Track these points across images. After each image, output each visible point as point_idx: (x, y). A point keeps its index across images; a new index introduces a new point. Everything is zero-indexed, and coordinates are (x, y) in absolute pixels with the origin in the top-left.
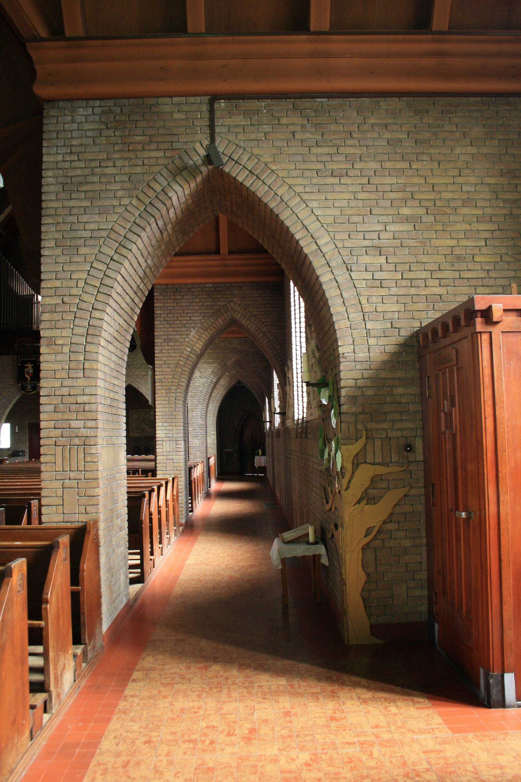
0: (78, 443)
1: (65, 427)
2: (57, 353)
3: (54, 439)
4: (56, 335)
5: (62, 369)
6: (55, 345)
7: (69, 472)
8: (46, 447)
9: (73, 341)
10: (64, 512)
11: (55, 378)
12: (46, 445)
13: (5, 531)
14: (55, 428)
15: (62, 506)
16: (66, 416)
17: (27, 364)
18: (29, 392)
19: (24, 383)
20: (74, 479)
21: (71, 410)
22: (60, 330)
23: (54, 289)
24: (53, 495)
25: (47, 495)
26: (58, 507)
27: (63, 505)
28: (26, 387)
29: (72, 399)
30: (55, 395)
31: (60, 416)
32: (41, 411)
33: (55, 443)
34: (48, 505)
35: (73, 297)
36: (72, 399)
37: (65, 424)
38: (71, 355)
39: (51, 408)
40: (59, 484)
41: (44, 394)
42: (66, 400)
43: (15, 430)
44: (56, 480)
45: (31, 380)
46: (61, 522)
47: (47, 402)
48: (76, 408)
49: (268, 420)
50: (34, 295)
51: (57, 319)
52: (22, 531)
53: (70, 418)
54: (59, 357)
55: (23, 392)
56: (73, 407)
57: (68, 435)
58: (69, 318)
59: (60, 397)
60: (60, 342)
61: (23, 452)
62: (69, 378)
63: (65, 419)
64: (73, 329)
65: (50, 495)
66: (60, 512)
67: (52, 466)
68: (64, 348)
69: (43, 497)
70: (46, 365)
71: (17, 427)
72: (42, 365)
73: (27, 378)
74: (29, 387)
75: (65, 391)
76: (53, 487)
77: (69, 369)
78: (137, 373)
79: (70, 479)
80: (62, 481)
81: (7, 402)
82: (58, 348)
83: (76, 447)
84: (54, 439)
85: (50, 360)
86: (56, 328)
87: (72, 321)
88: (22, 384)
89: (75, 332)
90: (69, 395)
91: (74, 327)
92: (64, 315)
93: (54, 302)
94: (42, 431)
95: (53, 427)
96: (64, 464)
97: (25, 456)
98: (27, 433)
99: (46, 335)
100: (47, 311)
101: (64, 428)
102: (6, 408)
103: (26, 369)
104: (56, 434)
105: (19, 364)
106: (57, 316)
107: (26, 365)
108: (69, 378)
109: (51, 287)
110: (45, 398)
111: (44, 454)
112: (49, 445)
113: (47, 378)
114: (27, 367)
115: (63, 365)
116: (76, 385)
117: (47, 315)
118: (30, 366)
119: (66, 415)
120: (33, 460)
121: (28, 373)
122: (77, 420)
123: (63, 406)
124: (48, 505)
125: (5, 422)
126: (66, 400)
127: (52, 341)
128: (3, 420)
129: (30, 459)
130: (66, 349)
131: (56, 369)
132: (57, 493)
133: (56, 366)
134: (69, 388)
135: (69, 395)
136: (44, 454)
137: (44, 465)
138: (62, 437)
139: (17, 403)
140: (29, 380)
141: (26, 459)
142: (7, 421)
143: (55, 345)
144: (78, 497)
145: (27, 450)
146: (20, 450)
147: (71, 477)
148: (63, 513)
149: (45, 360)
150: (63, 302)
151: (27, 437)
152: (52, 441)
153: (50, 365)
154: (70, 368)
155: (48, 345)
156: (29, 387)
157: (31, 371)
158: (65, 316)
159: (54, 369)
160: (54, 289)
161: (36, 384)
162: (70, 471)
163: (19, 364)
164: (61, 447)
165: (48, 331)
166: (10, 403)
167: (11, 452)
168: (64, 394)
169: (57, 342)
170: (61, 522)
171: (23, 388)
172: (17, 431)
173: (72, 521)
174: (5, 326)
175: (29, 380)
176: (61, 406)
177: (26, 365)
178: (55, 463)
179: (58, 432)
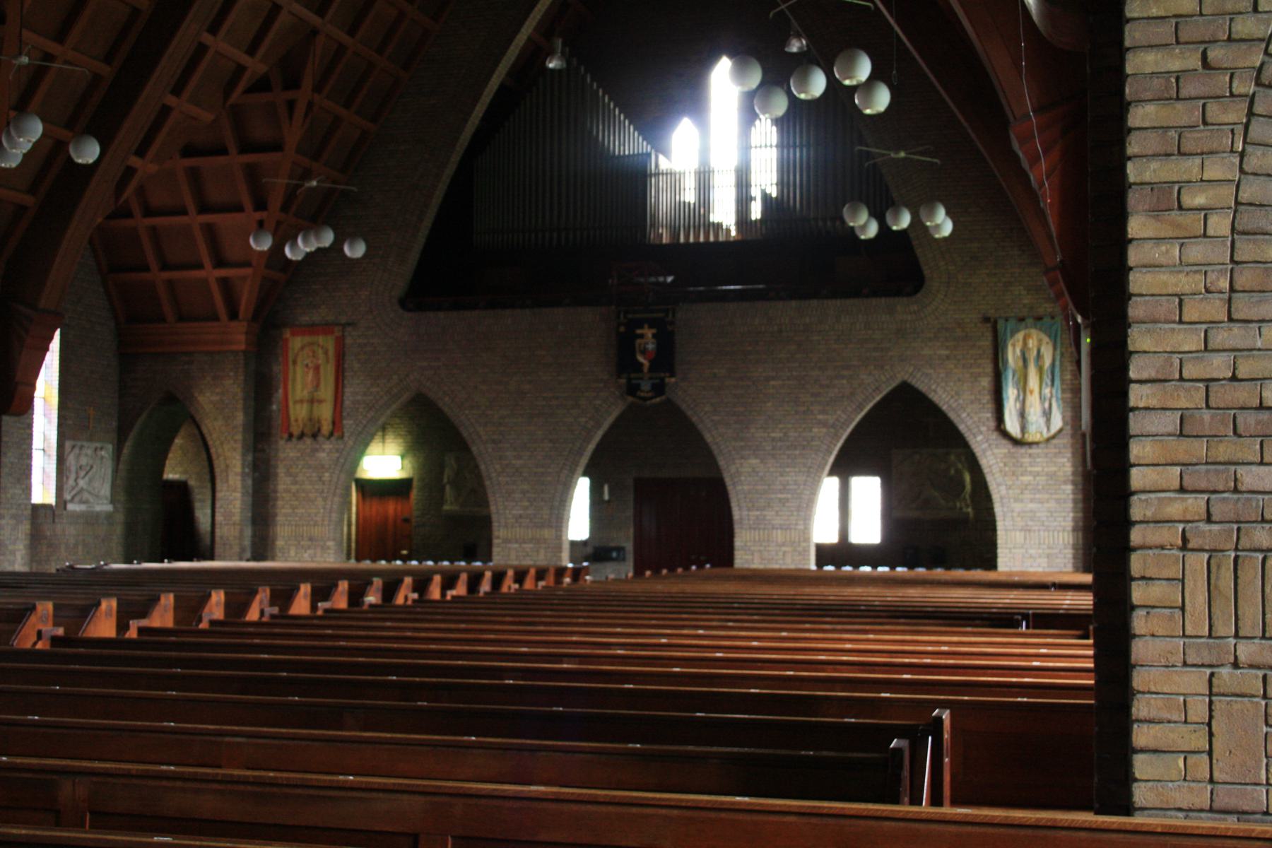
0: (1265, 545)
1: (1221, 488)
2: (1183, 240)
3: (1180, 527)
4: (1185, 178)
5: (1208, 291)
6: (1180, 208)
7: (1232, 641)
8: (1150, 552)
9: (1245, 196)
10: (1216, 775)
11: (1181, 322)
12: (1150, 548)
13: (1022, 832)
14: (1182, 490)
15: (1205, 757)
16: (1224, 451)
17: (642, 327)
18: (645, 399)
19: (633, 376)
20: (1251, 666)
21: (1241, 430)
22: (1198, 160)
23: (1173, 21)
24: (1175, 718)
25: (1153, 714)
26: (1192, 759)
27: (1210, 753)
28: (638, 387)
29: (1244, 395)
30: (1181, 379)
31: (1199, 449)
32: (1132, 432)
33: (1185, 539)
34: (1155, 751)
35: (1244, 46)
36: (1244, 395)
37: (1221, 480)
38: (1238, 245)
39: (1170, 422)
40: (1195, 681)
41: (1145, 376)
42: (1223, 394)
43: (602, 493)
44: (1185, 664)
45: (651, 369)
46: (1202, 810)
47: (1153, 402)
48: (1258, 422)
49: (448, 488)
50: (649, 155)
51: (1185, 121)
52: (1083, 834)
53: (1239, 456)
54: (1196, 252)
55: (630, 399)
56: (1248, 421)
57: (1232, 516)
58: (1231, 117)
59: (1201, 385)
60: (1199, 199)
61: (620, 549)
62: (1231, 319)
63: (1221, 459)
64: (1242, 155)
65: (1167, 716)
66: (1199, 776)
67: (1171, 618)
68: (1213, 220)
69: (1138, 721)
70: (1149, 277)
71: (583, 487)
72: (1132, 276)
73: (641, 365)
74: (646, 386)
75: (1218, 366)
76: (1174, 689)
77: (1232, 290)
78: (927, 352)
79: (1236, 665)
80: (1208, 671)
81: (592, 423)
82: (1193, 222)
83: (1260, 556)
84: (1180, 527)
85: (1163, 260)
86: (1180, 153)
87: (1239, 130)
88: (629, 380)
89: (1252, 163)
90: (1234, 378)
91: (1249, 149)
92: (1209, 107)
93: (1176, 65)
94: (1134, 499)
95: (1176, 485)
96: (1217, 612)
97: (624, 559)
98: (631, 504)
99: (1147, 177)
100: (1148, 95)
101: (1215, 492)
102: (587, 440)
103: (638, 341)
104: (1186, 510)
105: (622, 329)
106: (1183, 114)
107: (639, 331)
108: (1231, 319)
109: (1162, 14)
110: (1146, 389)
111: (1143, 578)
112: (1163, 548)
113: (1155, 321)
114: (642, 336)
115: (1212, 276)
116: (1259, 344)
117: (1150, 108)
118: (649, 333)
119: (1221, 448)
120: (648, 573)
121: (644, 352)
122: (1262, 463)
123: (1212, 417)
124: (1155, 751)
125: (831, 473)
126: (1223, 394)
127: (1169, 199)
128: (581, 469)
129: (639, 572)
130: (1220, 225)
131: (1187, 289)
132: (1190, 712)
133: (1185, 283)
134: (1232, 355)
135: (1234, 378)
136: (1143, 578)
137: (1142, 612)
138: (1209, 520)
139: (614, 426)
140: (646, 369)
141: (627, 569)
142: (584, 474)
143: (1180, 208)
144: (1265, 729)
145: (629, 546)
146: (612, 544)
147: (1242, 658)
148: (1211, 781)
149: (1145, 262)
150: (1205, 63)
151: (630, 513)
152: (1172, 535)
153: (1164, 277)
154: (1237, 287)
155: (1156, 211)
156: (646, 386)
157: (651, 347)
158: (1214, 110)
159: (1178, 290)
160: (1173, 21)
161: (662, 380)
162: (1236, 636)
163: (622, 329)
164: (1206, 556)
165: (1154, 165)
166: (598, 425)
167: (589, 550)
168: (1215, 375)
169: (1188, 201)
170: (1202, 810)
171: (632, 390)
172: (606, 497)
173: (1246, 808)
174: (555, 235)
175: (646, 369)
176: (1207, 415)
177: (639, 331)
178: (1183, 608)
179: (1195, 504)
